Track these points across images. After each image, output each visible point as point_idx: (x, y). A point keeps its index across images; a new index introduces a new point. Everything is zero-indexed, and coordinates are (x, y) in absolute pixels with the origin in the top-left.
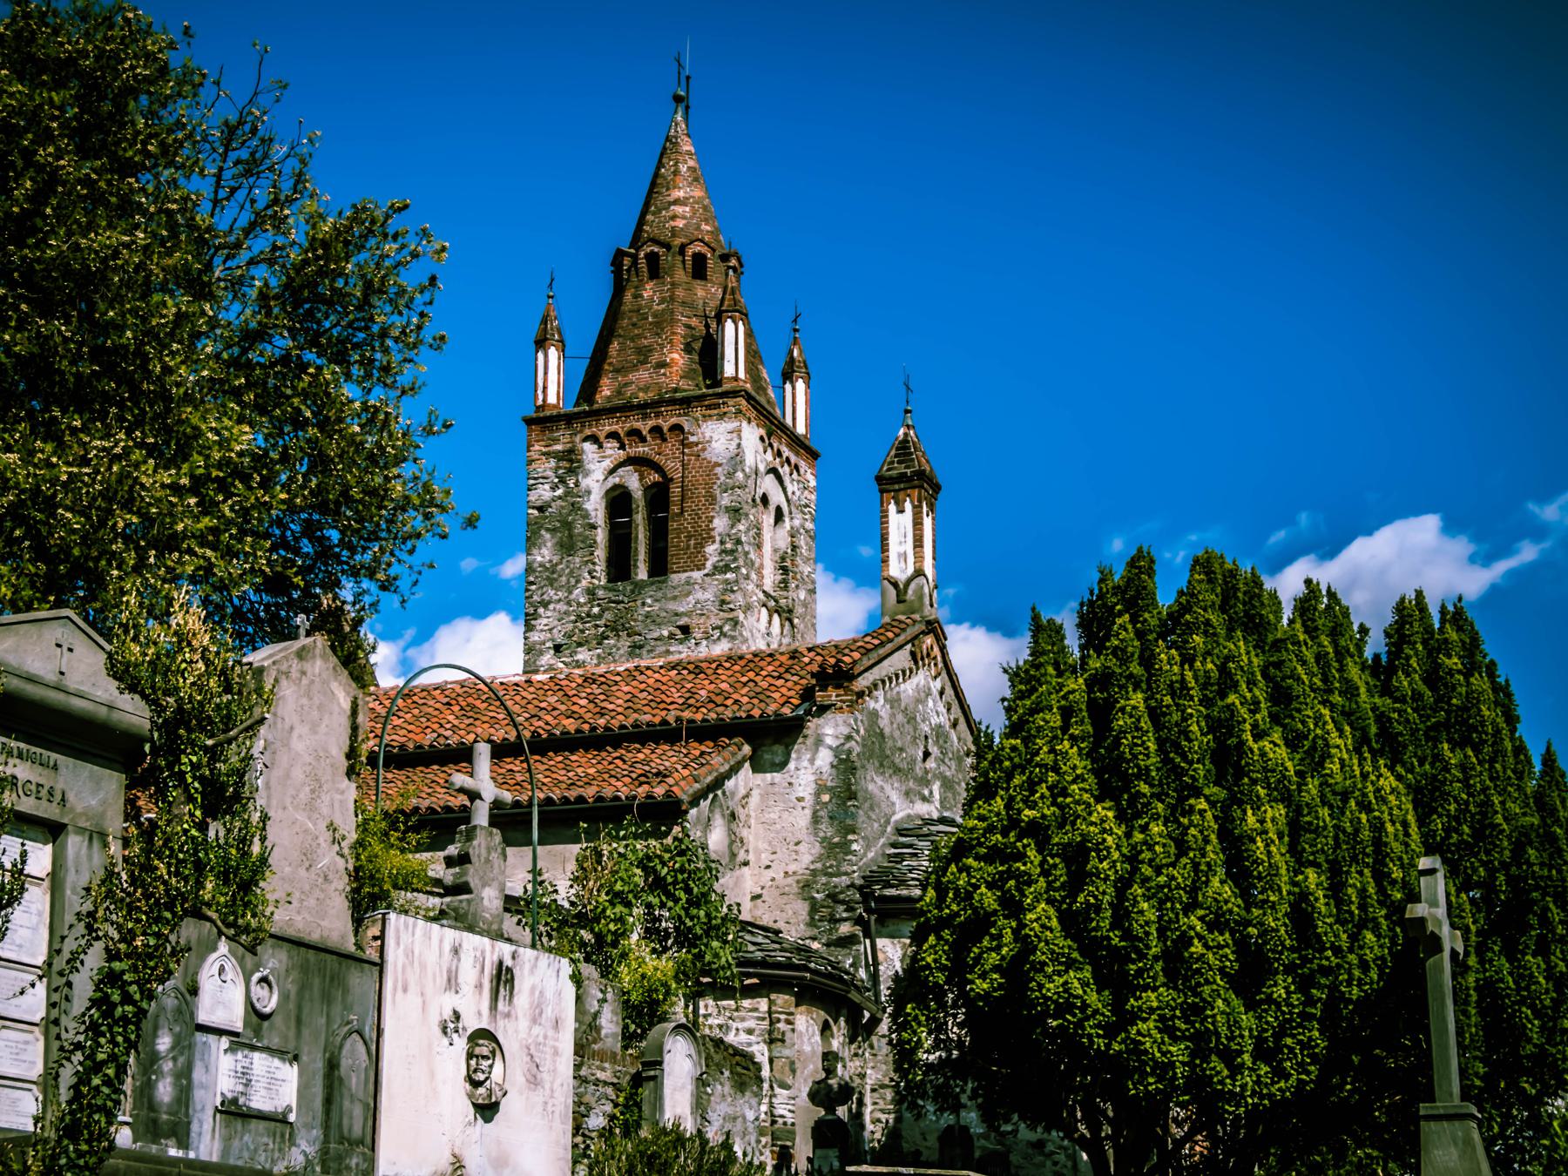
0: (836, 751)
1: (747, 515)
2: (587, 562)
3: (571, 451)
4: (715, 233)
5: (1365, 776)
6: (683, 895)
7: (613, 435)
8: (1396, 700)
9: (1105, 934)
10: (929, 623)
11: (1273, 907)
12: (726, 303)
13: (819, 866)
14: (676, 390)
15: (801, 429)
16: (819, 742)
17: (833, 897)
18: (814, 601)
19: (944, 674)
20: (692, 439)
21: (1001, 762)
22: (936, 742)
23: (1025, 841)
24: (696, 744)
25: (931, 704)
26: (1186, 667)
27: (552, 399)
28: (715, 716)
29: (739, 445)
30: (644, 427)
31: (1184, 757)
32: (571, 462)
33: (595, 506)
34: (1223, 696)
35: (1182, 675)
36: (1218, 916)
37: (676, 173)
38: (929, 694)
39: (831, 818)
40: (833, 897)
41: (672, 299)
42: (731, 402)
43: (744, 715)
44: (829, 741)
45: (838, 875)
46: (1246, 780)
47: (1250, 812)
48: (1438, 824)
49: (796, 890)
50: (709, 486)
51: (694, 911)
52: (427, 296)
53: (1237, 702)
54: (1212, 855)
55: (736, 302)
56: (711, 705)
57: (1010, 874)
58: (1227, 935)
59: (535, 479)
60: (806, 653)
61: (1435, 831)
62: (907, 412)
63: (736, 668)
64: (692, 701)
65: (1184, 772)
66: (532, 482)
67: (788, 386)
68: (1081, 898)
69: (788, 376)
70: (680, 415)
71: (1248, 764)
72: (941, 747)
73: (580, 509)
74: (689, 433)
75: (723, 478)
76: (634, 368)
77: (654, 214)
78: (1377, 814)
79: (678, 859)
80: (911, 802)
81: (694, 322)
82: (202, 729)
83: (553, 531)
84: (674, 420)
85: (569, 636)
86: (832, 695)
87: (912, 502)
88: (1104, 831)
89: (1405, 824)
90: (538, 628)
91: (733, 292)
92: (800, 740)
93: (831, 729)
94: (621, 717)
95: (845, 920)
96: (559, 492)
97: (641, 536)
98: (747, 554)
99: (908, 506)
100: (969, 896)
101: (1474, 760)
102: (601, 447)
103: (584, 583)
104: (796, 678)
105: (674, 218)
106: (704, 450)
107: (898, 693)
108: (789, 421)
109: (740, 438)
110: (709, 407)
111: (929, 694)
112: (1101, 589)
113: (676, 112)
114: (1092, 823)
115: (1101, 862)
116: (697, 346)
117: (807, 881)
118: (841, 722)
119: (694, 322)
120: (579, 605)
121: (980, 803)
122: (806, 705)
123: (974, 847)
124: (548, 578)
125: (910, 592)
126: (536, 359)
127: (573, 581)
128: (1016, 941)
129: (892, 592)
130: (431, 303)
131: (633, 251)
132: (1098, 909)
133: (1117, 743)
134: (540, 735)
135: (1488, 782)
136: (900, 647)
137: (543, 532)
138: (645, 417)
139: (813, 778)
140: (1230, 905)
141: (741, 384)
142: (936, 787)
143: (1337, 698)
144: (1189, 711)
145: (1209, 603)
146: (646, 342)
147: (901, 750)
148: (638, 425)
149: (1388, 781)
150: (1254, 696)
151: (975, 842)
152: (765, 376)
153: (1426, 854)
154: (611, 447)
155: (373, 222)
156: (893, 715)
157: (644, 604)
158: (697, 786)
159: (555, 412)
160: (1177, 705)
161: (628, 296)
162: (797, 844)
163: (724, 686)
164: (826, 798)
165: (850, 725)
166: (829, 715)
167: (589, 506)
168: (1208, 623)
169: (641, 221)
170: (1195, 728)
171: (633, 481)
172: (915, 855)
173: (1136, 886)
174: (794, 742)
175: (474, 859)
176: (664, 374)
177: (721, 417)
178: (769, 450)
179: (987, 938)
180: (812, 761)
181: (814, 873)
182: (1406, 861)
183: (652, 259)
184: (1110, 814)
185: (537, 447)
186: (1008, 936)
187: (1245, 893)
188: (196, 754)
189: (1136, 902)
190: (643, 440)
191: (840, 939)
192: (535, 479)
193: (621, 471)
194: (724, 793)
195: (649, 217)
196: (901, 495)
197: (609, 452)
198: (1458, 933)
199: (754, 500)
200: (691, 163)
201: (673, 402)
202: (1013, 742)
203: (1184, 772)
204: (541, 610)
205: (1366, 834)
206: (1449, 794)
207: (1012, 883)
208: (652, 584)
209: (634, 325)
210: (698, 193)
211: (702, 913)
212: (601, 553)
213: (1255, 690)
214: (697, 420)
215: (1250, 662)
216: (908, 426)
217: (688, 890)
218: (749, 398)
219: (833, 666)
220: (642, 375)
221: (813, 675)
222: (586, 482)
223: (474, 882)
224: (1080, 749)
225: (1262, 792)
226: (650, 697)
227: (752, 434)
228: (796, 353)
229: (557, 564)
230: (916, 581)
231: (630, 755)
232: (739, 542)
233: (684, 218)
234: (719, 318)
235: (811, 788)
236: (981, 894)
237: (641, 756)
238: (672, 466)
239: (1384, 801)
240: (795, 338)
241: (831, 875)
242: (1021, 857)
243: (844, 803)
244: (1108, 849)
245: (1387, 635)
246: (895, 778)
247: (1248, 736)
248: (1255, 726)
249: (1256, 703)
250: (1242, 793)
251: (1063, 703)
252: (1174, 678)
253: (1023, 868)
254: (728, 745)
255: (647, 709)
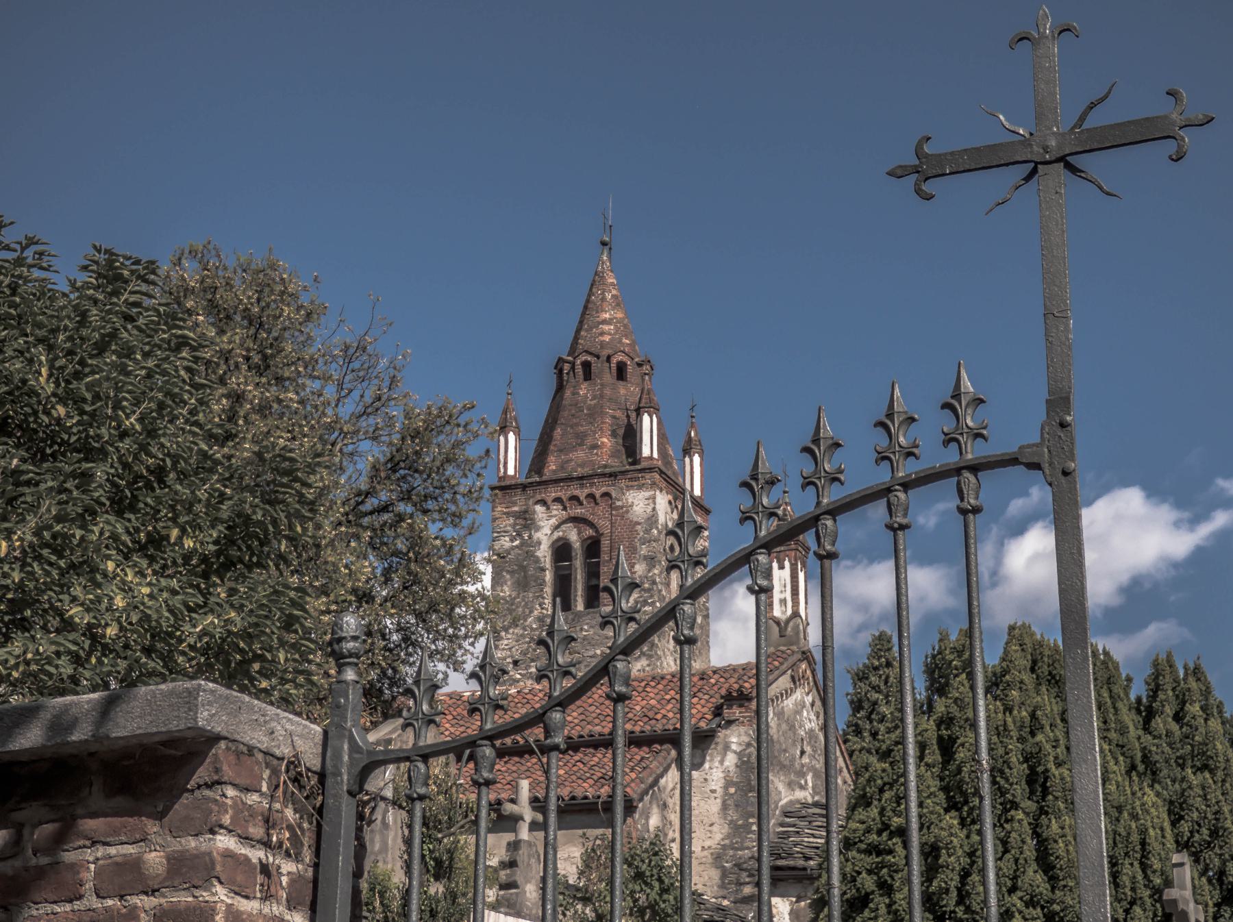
0: (740, 755)
1: (660, 562)
2: (538, 597)
3: (526, 512)
4: (632, 345)
5: (1133, 794)
6: (656, 884)
7: (558, 500)
8: (1155, 737)
9: (952, 908)
10: (804, 653)
11: (1071, 890)
12: (643, 401)
13: (727, 842)
14: (605, 466)
15: (697, 492)
16: (727, 747)
17: (739, 866)
18: (708, 624)
19: (814, 690)
20: (619, 503)
21: (875, 780)
22: (809, 743)
23: (894, 840)
24: (636, 750)
25: (805, 714)
26: (1007, 714)
27: (511, 472)
28: (649, 728)
29: (654, 509)
30: (582, 494)
31: (1007, 780)
32: (526, 521)
33: (544, 552)
34: (1033, 734)
35: (1005, 721)
36: (1032, 897)
37: (604, 299)
38: (804, 706)
39: (736, 806)
40: (739, 866)
41: (602, 396)
42: (648, 476)
43: (671, 728)
44: (734, 747)
45: (742, 849)
46: (1050, 797)
47: (1054, 821)
48: (1185, 827)
49: (710, 860)
50: (631, 540)
51: (665, 896)
52: (483, 463)
53: (1044, 740)
54: (1028, 853)
55: (651, 400)
56: (646, 719)
57: (882, 865)
58: (1039, 910)
59: (498, 532)
60: (711, 675)
61: (1183, 833)
62: (785, 492)
63: (660, 687)
64: (630, 715)
65: (1007, 791)
66: (496, 535)
67: (687, 460)
68: (935, 883)
69: (687, 451)
70: (608, 485)
71: (1052, 786)
72: (812, 747)
73: (533, 556)
74: (616, 499)
75: (642, 534)
76: (573, 448)
77: (587, 331)
78: (1142, 821)
79: (653, 858)
80: (793, 790)
81: (618, 414)
82: (435, 827)
83: (512, 573)
84: (604, 489)
85: (524, 653)
86: (736, 712)
87: (790, 561)
88: (952, 835)
89: (1162, 829)
90: (501, 647)
91: (649, 393)
92: (713, 746)
93: (736, 738)
94: (578, 728)
95: (748, 883)
96: (517, 543)
97: (579, 577)
98: (661, 591)
99: (787, 564)
100: (854, 880)
101: (1211, 781)
102: (548, 508)
103: (536, 613)
104: (706, 697)
105: (602, 334)
106: (627, 512)
107: (783, 708)
108: (688, 486)
109: (655, 503)
110: (631, 480)
111: (804, 706)
112: (940, 647)
113: (602, 253)
114: (942, 829)
115: (949, 856)
116: (621, 432)
117: (719, 854)
118: (743, 733)
119: (618, 414)
120: (532, 629)
121: (861, 810)
122: (718, 719)
123: (855, 843)
124: (508, 609)
125: (789, 629)
126: (499, 441)
127: (527, 611)
128: (889, 913)
129: (776, 629)
130: (485, 467)
131: (570, 358)
132: (947, 891)
133: (959, 771)
134: (518, 742)
135: (1221, 797)
136: (784, 673)
137: (505, 574)
138: (582, 486)
139: (722, 775)
140: (1041, 889)
141: (655, 462)
142: (809, 778)
143: (1113, 735)
144: (1010, 747)
145: (1023, 667)
146: (582, 429)
147: (785, 751)
148: (577, 492)
149: (1150, 797)
150: (1055, 735)
151: (857, 840)
152: (671, 452)
153: (1178, 851)
154: (556, 510)
155: (450, 416)
156: (779, 725)
157: (582, 629)
158: (643, 786)
159: (513, 482)
160: (1001, 742)
161: (568, 393)
162: (711, 825)
163: (653, 702)
164: (732, 790)
165: (749, 735)
166: (734, 727)
167: (539, 554)
168: (1021, 682)
169: (576, 337)
170: (1014, 759)
171: (573, 536)
172: (798, 832)
173: (974, 875)
174: (708, 748)
175: (520, 863)
176: (597, 454)
177: (640, 487)
178: (675, 511)
179: (867, 910)
180: (722, 762)
181: (724, 847)
182: (1163, 856)
183: (587, 366)
184: (955, 822)
185: (499, 509)
186: (883, 910)
187: (1053, 880)
188: (431, 843)
189: (974, 887)
190: (581, 504)
191: (745, 898)
192: (498, 532)
193: (563, 527)
194: (659, 789)
195: (583, 333)
196: (782, 555)
197: (555, 512)
198: (1200, 907)
199: (664, 550)
200: (614, 292)
201: (604, 475)
202: (883, 765)
203: (1007, 791)
204: (503, 634)
205: (1135, 838)
206: (1192, 806)
207: (885, 871)
208: (588, 614)
209: (573, 415)
210: (620, 315)
211: (671, 898)
212: (548, 590)
213: (1056, 730)
214: (622, 489)
215: (1052, 710)
216: (786, 504)
217: (660, 880)
218: (661, 472)
219: (737, 691)
220: (580, 455)
221: (722, 697)
222: (538, 535)
223: (519, 879)
224: (932, 773)
225: (1062, 806)
226: (598, 711)
227: (662, 500)
228: (693, 434)
229: (515, 598)
230: (794, 621)
231: (586, 758)
232: (654, 582)
233: (610, 334)
234: (639, 412)
235: (721, 783)
236: (863, 878)
237: (596, 759)
238: (604, 524)
239: (1148, 812)
240: (692, 423)
241: (737, 849)
242: (890, 852)
243: (746, 795)
244: (954, 848)
245: (1147, 683)
246: (781, 773)
247: (1051, 766)
248: (1056, 758)
249: (1057, 741)
250: (1048, 806)
251: (920, 738)
252: (999, 723)
253: (893, 860)
254: (660, 751)
255: (597, 721)
